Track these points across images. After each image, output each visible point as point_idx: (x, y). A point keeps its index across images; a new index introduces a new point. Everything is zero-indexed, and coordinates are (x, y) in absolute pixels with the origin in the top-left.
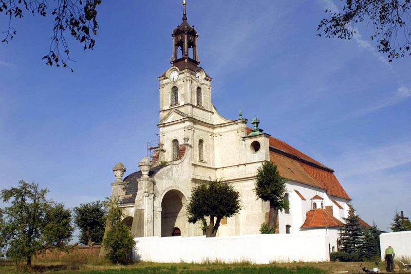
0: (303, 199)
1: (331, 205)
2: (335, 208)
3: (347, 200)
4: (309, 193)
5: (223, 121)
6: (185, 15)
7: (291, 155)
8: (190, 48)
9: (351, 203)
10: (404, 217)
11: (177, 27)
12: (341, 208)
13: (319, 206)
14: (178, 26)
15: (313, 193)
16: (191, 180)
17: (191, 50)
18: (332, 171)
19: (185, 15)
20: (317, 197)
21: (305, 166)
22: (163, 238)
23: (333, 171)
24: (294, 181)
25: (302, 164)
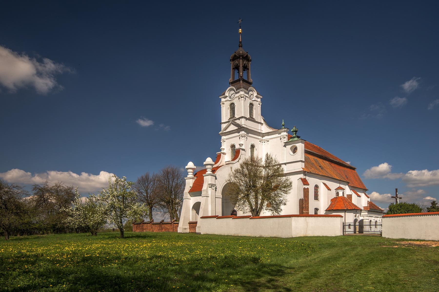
0: (329, 189)
1: (351, 194)
2: (354, 196)
4: (334, 185)
7: (322, 156)
12: (359, 196)
13: (341, 194)
20: (340, 188)
21: (333, 165)
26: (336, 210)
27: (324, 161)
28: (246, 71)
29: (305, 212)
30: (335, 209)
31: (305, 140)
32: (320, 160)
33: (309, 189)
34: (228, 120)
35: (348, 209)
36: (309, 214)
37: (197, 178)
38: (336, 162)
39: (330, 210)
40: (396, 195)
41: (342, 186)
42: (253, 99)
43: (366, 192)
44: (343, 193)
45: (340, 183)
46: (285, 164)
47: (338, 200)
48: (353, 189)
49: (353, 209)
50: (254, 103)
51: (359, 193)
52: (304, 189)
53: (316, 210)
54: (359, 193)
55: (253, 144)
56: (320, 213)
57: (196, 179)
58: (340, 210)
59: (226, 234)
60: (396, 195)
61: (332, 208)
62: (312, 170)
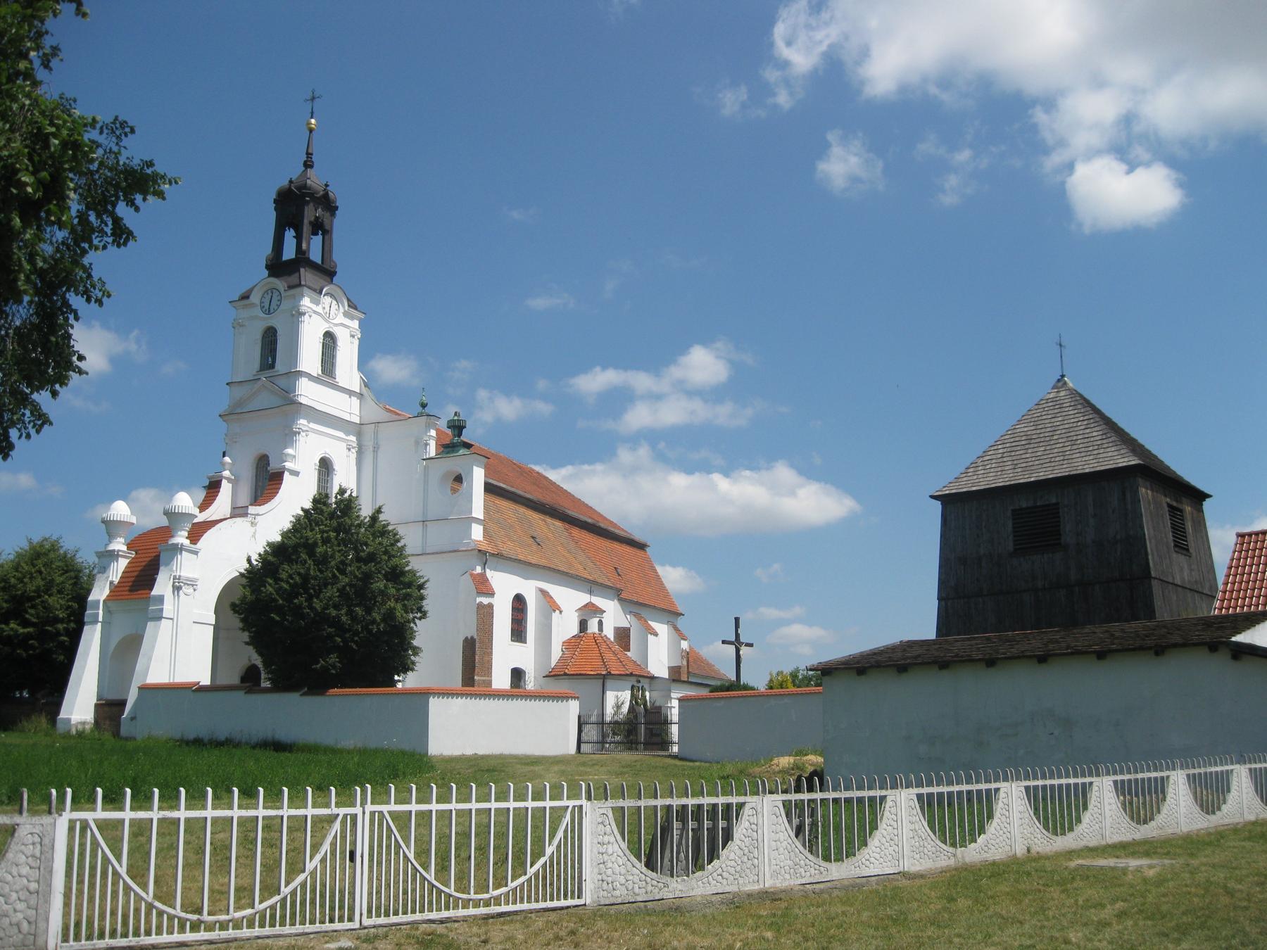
1: (626, 625)
3: (671, 614)
4: (571, 600)
5: (121, 880)
6: (309, 154)
7: (543, 505)
8: (317, 234)
9: (680, 622)
10: (733, 647)
11: (286, 183)
14: (291, 182)
15: (583, 598)
16: (154, 162)
17: (317, 241)
18: (641, 546)
19: (309, 154)
21: (576, 532)
22: (122, 817)
23: (1207, 496)
24: (544, 567)
25: (567, 526)
26: (577, 675)
27: (549, 520)
28: (320, 237)
29: (480, 678)
30: (572, 673)
31: (486, 457)
32: (535, 517)
33: (493, 606)
34: (255, 375)
35: (613, 672)
36: (493, 687)
37: (139, 556)
38: (586, 522)
39: (559, 675)
40: (737, 635)
41: (599, 601)
42: (335, 322)
43: (677, 620)
44: (600, 623)
45: (591, 592)
46: (413, 555)
47: (586, 641)
48: (636, 609)
49: (628, 673)
50: (339, 332)
51: (652, 624)
52: (480, 606)
53: (517, 675)
54: (652, 624)
55: (328, 456)
56: (530, 684)
57: (133, 558)
58: (588, 675)
59: (590, 505)
60: (737, 635)
61: (566, 671)
62: (508, 548)
